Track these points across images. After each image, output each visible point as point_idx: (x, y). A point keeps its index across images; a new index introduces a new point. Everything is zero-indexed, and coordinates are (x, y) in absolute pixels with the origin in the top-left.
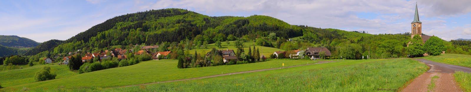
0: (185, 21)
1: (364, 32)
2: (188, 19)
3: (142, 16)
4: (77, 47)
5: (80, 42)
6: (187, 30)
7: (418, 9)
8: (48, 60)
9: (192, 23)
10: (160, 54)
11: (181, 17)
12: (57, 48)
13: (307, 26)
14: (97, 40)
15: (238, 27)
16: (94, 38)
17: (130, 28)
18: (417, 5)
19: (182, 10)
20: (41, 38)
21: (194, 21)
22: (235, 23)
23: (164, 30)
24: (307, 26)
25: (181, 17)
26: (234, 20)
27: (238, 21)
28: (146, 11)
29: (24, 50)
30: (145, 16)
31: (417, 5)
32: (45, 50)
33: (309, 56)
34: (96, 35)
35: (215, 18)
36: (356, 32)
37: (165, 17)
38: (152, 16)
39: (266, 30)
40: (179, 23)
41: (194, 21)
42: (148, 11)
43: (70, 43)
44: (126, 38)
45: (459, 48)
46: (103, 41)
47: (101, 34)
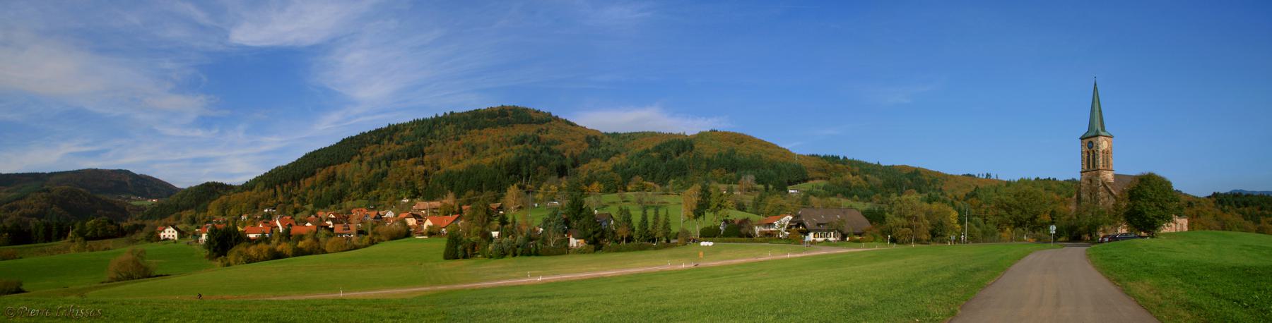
0: (539, 139)
1: (988, 175)
2: (548, 136)
3: (423, 128)
4: (262, 203)
5: (272, 191)
6: (535, 161)
7: (1102, 107)
8: (169, 232)
9: (553, 147)
10: (431, 224)
11: (531, 130)
12: (217, 202)
13: (845, 158)
14: (314, 187)
15: (664, 158)
16: (308, 182)
17: (390, 159)
18: (1095, 85)
19: (538, 112)
20: (184, 177)
21: (560, 142)
22: (658, 149)
23: (474, 161)
24: (845, 158)
25: (531, 130)
26: (657, 143)
27: (668, 144)
28: (434, 117)
29: (143, 205)
30: (430, 130)
31: (1095, 85)
32: (188, 208)
33: (801, 232)
34: (313, 174)
35: (615, 135)
36: (969, 175)
37: (482, 128)
38: (450, 128)
39: (734, 170)
40: (522, 142)
41: (560, 142)
42: (441, 115)
43: (247, 193)
44: (379, 184)
45: (1233, 217)
46: (327, 190)
47: (324, 171)
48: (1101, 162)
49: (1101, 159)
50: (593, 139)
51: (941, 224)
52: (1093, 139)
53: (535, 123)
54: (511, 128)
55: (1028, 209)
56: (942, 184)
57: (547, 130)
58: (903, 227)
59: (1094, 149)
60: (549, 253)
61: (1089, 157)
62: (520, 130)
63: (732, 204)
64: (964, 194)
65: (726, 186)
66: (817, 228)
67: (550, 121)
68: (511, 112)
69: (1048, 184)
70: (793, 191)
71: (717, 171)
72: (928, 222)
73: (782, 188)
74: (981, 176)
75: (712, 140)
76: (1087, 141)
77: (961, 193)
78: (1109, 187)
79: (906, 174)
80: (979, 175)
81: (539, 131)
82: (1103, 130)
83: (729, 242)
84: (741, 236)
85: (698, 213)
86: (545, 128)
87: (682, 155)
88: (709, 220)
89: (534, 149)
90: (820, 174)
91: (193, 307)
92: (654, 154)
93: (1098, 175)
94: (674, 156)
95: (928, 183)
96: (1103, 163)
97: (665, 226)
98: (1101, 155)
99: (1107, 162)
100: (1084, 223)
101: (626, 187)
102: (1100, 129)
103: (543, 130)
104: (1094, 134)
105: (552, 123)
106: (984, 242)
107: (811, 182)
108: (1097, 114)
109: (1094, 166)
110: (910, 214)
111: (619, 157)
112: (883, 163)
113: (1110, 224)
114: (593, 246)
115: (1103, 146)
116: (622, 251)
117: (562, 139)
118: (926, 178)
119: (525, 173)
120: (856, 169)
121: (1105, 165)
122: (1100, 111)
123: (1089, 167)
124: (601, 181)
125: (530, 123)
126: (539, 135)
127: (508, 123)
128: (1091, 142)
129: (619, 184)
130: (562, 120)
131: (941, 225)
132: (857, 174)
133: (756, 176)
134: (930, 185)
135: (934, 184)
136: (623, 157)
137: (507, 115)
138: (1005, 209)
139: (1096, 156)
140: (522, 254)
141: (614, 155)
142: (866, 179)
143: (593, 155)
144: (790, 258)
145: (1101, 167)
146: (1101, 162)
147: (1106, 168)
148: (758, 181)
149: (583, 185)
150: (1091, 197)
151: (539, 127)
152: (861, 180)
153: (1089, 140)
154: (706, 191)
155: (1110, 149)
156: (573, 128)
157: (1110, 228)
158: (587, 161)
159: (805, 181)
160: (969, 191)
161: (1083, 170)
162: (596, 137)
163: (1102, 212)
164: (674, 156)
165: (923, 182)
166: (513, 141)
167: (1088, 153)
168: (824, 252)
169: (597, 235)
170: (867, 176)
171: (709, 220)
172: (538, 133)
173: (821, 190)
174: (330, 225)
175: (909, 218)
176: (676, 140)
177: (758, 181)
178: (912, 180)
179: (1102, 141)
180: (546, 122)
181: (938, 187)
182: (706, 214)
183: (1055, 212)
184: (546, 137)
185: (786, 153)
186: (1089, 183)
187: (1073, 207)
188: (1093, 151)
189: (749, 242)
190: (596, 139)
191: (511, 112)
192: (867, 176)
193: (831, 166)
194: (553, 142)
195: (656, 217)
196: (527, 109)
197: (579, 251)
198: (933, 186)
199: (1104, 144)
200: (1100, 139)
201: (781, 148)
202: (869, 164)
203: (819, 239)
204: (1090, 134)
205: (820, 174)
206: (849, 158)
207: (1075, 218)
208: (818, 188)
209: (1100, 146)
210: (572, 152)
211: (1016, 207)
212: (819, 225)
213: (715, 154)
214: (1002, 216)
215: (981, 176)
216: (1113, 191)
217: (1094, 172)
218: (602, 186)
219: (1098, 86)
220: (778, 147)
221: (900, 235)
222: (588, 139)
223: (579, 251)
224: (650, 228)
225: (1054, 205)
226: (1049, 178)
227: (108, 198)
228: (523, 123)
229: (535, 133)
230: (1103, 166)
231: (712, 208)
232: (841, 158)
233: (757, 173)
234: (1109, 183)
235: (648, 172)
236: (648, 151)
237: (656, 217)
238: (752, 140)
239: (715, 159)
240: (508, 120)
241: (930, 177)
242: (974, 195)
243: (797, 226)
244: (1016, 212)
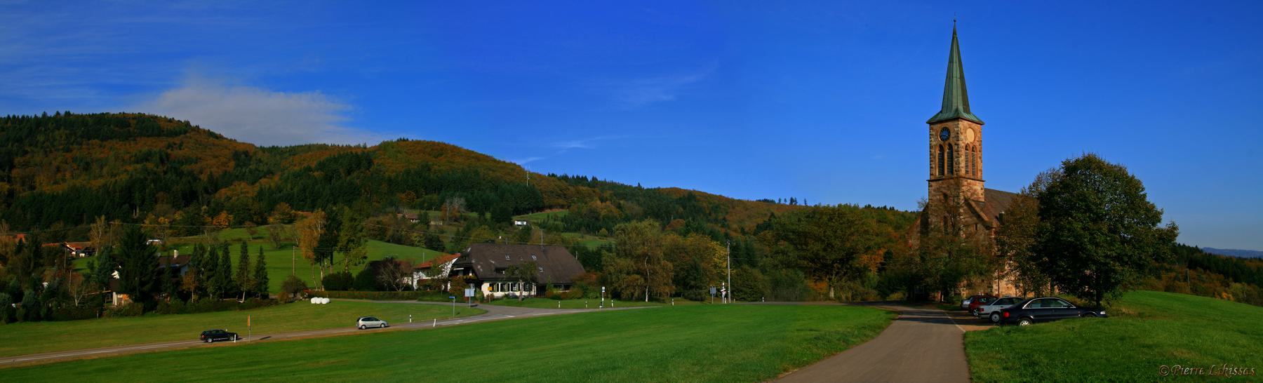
1: (792, 200)
2: (181, 152)
7: (959, 43)
11: (158, 145)
13: (594, 179)
15: (328, 179)
18: (955, 33)
19: (171, 121)
22: (322, 166)
24: (594, 179)
25: (158, 145)
27: (335, 160)
31: (955, 33)
35: (274, 149)
48: (963, 164)
49: (962, 158)
50: (243, 156)
51: (695, 267)
52: (949, 125)
53: (164, 135)
54: (132, 142)
55: (837, 243)
56: (727, 213)
57: (181, 145)
58: (628, 274)
59: (951, 140)
60: (70, 316)
61: (942, 155)
62: (144, 145)
63: (418, 239)
64: (755, 225)
65: (416, 212)
66: (495, 275)
67: (186, 132)
68: (135, 121)
69: (883, 215)
70: (519, 223)
71: (403, 196)
72: (670, 265)
73: (503, 219)
74: (782, 202)
75: (399, 152)
76: (938, 127)
77: (750, 225)
78: (978, 209)
79: (677, 200)
80: (780, 200)
81: (169, 146)
82: (967, 110)
83: (362, 298)
84: (380, 288)
85: (323, 251)
86: (177, 142)
87: (355, 174)
88: (340, 263)
89: (155, 169)
90: (561, 201)
92: (316, 174)
93: (958, 186)
94: (343, 175)
95: (708, 212)
96: (967, 166)
97: (257, 272)
98: (963, 152)
99: (973, 165)
100: (934, 270)
101: (266, 219)
102: (961, 108)
103: (175, 144)
104: (950, 115)
105: (188, 135)
106: (776, 298)
107: (548, 211)
108: (956, 81)
109: (951, 171)
110: (639, 252)
111: (271, 178)
112: (645, 186)
113: (981, 274)
114: (140, 305)
116: (189, 313)
117: (200, 156)
119: (138, 202)
120: (607, 194)
121: (970, 169)
122: (962, 78)
123: (942, 172)
124: (230, 211)
125: (159, 135)
126: (169, 151)
127: (128, 137)
128: (947, 130)
129: (255, 214)
130: (204, 131)
131: (696, 269)
132: (607, 200)
133: (467, 200)
134: (710, 214)
136: (276, 178)
137: (129, 125)
138: (791, 241)
139: (955, 154)
140: (26, 318)
141: (265, 177)
142: (619, 207)
143: (237, 176)
144: (438, 328)
145: (963, 172)
146: (963, 164)
147: (970, 175)
148: (470, 207)
149: (206, 215)
150: (946, 223)
151: (171, 140)
152: (613, 208)
153: (944, 125)
154: (334, 220)
155: (977, 144)
156: (216, 141)
157: (979, 281)
158: (227, 185)
159: (540, 209)
160: (760, 221)
161: (933, 178)
162: (246, 153)
163: (967, 252)
164: (343, 175)
166: (133, 159)
167: (941, 148)
168: (511, 314)
169: (148, 287)
170: (622, 202)
171: (340, 263)
172: (168, 148)
173: (559, 223)
175: (638, 258)
176: (347, 155)
177: (470, 207)
178: (684, 208)
179: (965, 129)
180: (181, 133)
181: (721, 217)
182: (335, 254)
183: (891, 254)
184: (176, 153)
185: (516, 169)
186: (942, 197)
187: (914, 241)
188: (950, 145)
189: (387, 298)
190: (246, 156)
191: (135, 121)
192: (622, 202)
193: (571, 188)
194: (187, 160)
195: (244, 257)
196: (156, 117)
197: (121, 313)
198: (714, 215)
199: (968, 135)
200: (962, 124)
201: (499, 162)
202: (626, 187)
203: (499, 294)
204: (945, 116)
205: (561, 201)
206: (600, 179)
207: (918, 259)
208: (555, 220)
209: (962, 137)
210: (211, 173)
211: (817, 239)
212: (498, 270)
213: (401, 172)
214: (784, 253)
215: (782, 202)
216: (982, 214)
217: (952, 181)
218: (231, 217)
219: (959, 35)
220: (495, 161)
221: (623, 286)
222: (236, 155)
223: (121, 313)
224: (234, 276)
225: (890, 244)
226: (885, 207)
228: (148, 136)
229: (165, 149)
230: (967, 172)
231: (340, 245)
232: (590, 179)
233: (470, 196)
234: (977, 202)
235: (306, 198)
236: (309, 169)
237: (244, 257)
238: (455, 150)
239: (399, 179)
240: (129, 131)
241: (711, 203)
242: (767, 226)
243: (466, 272)
244: (815, 247)
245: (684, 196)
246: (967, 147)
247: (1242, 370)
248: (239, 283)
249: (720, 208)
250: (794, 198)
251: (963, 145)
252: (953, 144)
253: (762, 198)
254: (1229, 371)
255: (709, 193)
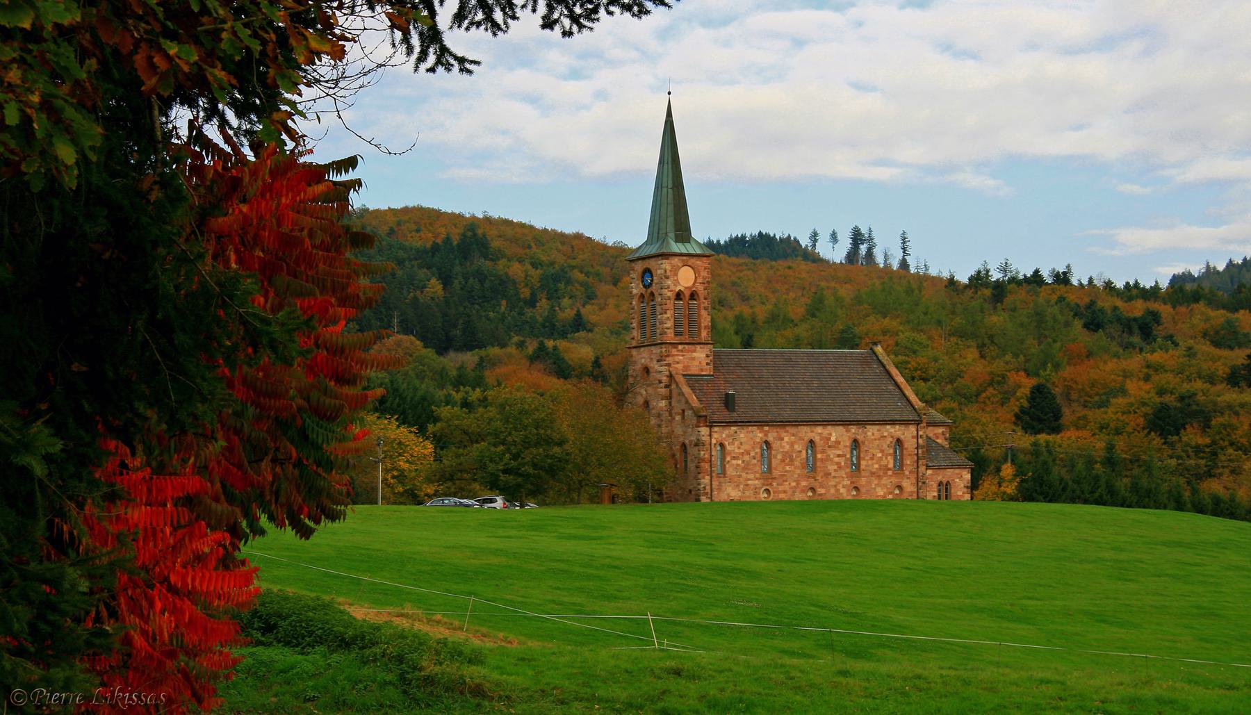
1: (857, 238)
52: (651, 264)
56: (590, 297)
80: (814, 237)
91: (872, 459)
115: (677, 282)
118: (516, 270)
128: (647, 271)
134: (532, 302)
135: (553, 296)
165: (502, 287)
174: (164, 696)
227: (795, 660)
230: (677, 334)
245: (448, 240)
246: (679, 296)
247: (146, 697)
248: (1153, 433)
249: (569, 282)
250: (864, 231)
251: (669, 294)
252: (656, 294)
253: (750, 231)
254: (124, 698)
255: (539, 224)
